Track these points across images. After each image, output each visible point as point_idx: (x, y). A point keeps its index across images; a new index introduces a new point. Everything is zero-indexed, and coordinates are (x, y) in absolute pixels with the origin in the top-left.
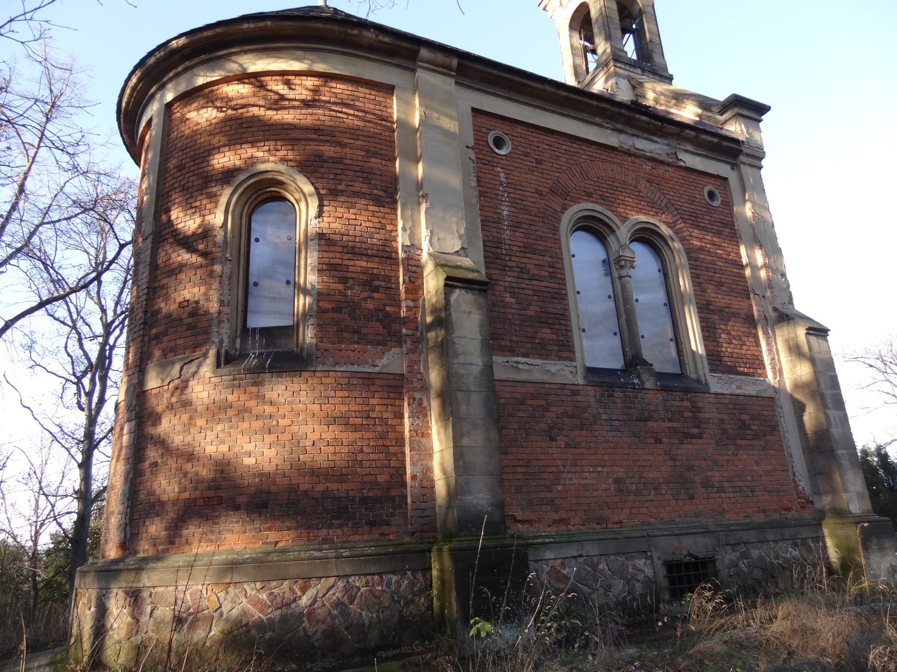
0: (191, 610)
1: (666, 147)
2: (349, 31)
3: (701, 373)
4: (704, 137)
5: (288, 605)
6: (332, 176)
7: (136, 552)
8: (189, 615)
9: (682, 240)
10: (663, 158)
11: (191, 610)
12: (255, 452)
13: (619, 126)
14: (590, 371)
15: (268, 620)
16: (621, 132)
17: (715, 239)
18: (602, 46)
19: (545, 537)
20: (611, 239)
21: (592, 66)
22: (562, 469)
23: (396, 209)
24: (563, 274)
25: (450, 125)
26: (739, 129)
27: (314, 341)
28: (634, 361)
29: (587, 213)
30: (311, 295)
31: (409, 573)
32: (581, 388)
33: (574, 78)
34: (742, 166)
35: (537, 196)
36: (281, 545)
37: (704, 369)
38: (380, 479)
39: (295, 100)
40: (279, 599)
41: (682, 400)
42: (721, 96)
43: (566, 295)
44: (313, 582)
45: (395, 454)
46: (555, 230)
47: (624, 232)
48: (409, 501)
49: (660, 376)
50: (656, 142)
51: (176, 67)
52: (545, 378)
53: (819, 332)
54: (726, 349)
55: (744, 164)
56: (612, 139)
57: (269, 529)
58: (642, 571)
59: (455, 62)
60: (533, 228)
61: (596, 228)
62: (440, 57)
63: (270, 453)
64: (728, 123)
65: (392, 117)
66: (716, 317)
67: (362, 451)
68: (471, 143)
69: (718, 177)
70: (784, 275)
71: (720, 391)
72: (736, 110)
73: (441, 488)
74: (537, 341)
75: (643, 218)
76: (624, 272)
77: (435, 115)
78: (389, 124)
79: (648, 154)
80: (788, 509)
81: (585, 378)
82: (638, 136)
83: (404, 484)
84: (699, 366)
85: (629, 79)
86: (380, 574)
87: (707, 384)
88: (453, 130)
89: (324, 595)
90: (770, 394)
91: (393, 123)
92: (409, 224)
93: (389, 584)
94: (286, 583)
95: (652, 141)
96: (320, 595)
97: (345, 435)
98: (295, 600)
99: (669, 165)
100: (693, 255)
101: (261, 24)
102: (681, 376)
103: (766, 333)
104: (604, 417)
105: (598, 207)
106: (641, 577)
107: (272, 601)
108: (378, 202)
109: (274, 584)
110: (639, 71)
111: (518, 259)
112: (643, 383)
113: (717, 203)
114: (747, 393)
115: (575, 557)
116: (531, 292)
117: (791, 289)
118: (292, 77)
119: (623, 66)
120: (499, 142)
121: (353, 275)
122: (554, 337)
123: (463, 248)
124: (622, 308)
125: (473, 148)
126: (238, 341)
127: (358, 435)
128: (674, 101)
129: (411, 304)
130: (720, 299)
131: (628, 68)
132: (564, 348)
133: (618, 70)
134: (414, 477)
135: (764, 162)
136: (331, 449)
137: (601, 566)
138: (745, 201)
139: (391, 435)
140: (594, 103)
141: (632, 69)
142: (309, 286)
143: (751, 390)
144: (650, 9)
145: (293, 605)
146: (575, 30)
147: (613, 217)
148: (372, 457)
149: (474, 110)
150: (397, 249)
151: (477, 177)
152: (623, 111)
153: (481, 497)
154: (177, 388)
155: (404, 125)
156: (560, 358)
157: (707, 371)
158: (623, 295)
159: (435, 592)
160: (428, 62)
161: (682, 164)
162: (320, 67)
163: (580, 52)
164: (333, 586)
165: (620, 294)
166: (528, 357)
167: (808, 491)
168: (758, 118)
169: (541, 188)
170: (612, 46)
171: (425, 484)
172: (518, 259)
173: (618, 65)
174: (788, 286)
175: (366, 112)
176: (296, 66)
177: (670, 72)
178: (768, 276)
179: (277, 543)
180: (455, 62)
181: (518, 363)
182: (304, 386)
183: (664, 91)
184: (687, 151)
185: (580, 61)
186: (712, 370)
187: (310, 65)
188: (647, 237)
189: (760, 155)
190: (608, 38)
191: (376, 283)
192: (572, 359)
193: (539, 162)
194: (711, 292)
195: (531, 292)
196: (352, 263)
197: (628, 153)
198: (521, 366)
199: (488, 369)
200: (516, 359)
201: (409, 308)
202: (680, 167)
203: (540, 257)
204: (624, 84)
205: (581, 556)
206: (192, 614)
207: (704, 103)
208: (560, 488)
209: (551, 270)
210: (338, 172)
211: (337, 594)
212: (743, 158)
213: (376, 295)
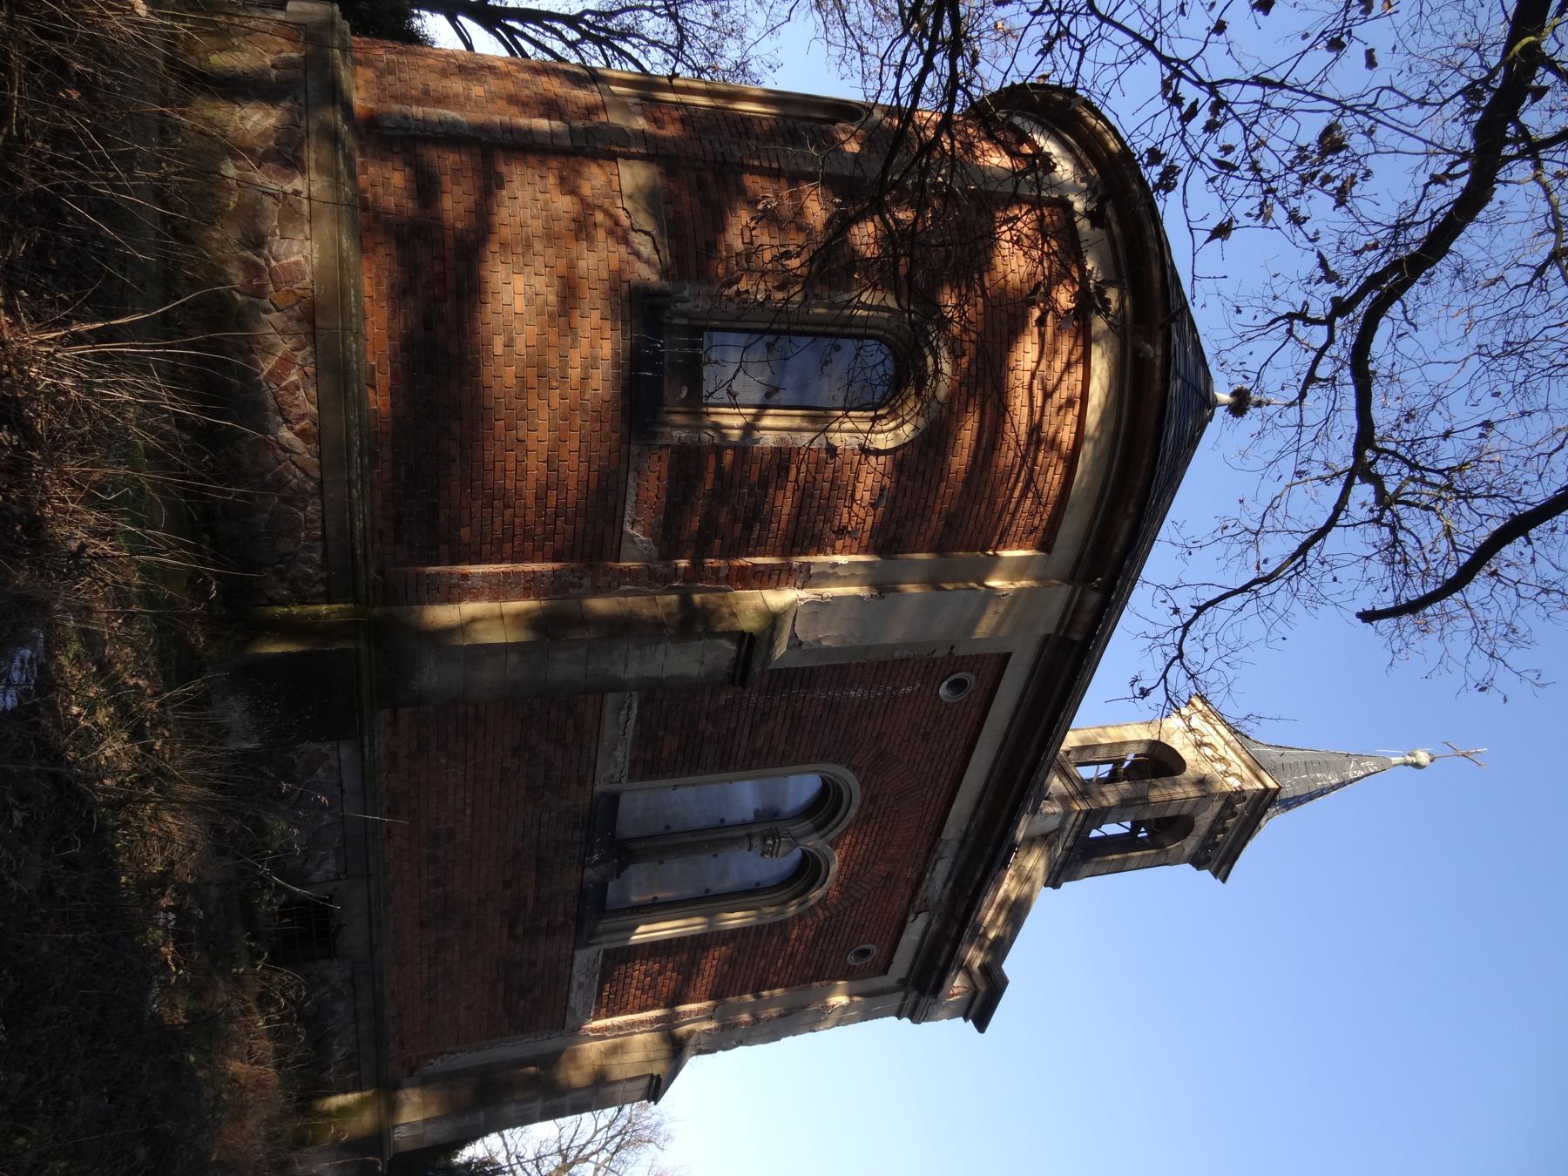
0: (273, 263)
1: (936, 898)
2: (1133, 501)
3: (604, 938)
4: (947, 948)
5: (280, 411)
6: (921, 467)
7: (353, 33)
8: (267, 260)
9: (800, 917)
10: (921, 894)
11: (273, 263)
12: (514, 293)
13: (970, 840)
14: (614, 799)
15: (259, 382)
16: (963, 842)
17: (799, 958)
18: (1111, 796)
19: (372, 745)
20: (807, 825)
22: (471, 763)
23: (865, 553)
24: (757, 767)
25: (984, 628)
27: (675, 441)
28: (624, 853)
29: (846, 797)
30: (743, 437)
31: (324, 575)
32: (589, 787)
33: (1077, 744)
34: (902, 994)
35: (875, 734)
36: (371, 393)
37: (610, 942)
38: (465, 532)
39: (1042, 414)
40: (289, 399)
41: (565, 915)
43: (727, 770)
44: (313, 446)
45: (500, 550)
46: (824, 757)
47: (813, 843)
48: (432, 569)
49: (603, 887)
50: (945, 886)
51: (1119, 224)
52: (606, 742)
53: (654, 1089)
54: (638, 971)
55: (905, 998)
56: (952, 830)
57: (394, 376)
58: (318, 867)
60: (828, 729)
61: (824, 807)
62: (1085, 618)
63: (509, 375)
65: (1004, 548)
66: (685, 957)
67: (506, 507)
68: (958, 652)
69: (890, 962)
70: (741, 1043)
71: (576, 962)
72: (982, 988)
73: (444, 614)
74: (661, 733)
75: (834, 868)
76: (757, 842)
77: (1001, 609)
78: (994, 544)
80: (402, 1044)
81: (603, 793)
82: (954, 863)
83: (456, 561)
84: (615, 936)
85: (1058, 831)
86: (323, 537)
87: (587, 945)
89: (294, 463)
90: (570, 1023)
91: (996, 549)
92: (841, 572)
93: (310, 549)
94: (314, 409)
95: (948, 880)
96: (295, 458)
97: (532, 484)
98: (287, 421)
99: (911, 901)
100: (778, 930)
101: (1157, 375)
102: (602, 910)
103: (658, 1019)
104: (545, 817)
105: (853, 811)
106: (309, 866)
107: (286, 388)
108: (876, 531)
109: (313, 392)
111: (782, 709)
112: (593, 866)
113: (851, 959)
114: (572, 995)
115: (341, 784)
116: (733, 725)
117: (720, 1053)
118: (1077, 411)
120: (958, 686)
121: (770, 496)
122: (665, 754)
123: (801, 643)
124: (705, 837)
125: (950, 654)
126: (684, 322)
127: (530, 502)
129: (722, 574)
130: (710, 965)
132: (647, 765)
133: (1074, 817)
134: (465, 576)
135: (906, 1021)
136: (511, 466)
137: (326, 817)
138: (850, 995)
139: (528, 545)
140: (1005, 812)
142: (757, 435)
143: (576, 1000)
145: (279, 419)
147: (845, 824)
148: (498, 520)
149: (1007, 656)
150: (807, 554)
151: (908, 659)
152: (990, 849)
153: (432, 676)
154: (617, 223)
155: (992, 564)
156: (633, 763)
157: (607, 946)
158: (723, 839)
159: (296, 610)
160: (1081, 601)
162: (1087, 448)
163: (1115, 755)
164: (307, 475)
165: (726, 835)
166: (637, 721)
167: (429, 1069)
168: (973, 1010)
169: (886, 739)
171: (455, 592)
172: (782, 709)
174: (724, 1049)
175: (1014, 514)
176: (1092, 419)
178: (740, 1024)
179: (374, 387)
180: (1077, 637)
181: (630, 708)
182: (607, 427)
184: (929, 924)
185: (1102, 754)
186: (607, 953)
187: (1092, 438)
188: (807, 871)
189: (917, 1014)
191: (757, 527)
192: (632, 777)
193: (926, 737)
194: (718, 952)
195: (733, 725)
196: (789, 494)
197: (931, 850)
198: (624, 712)
199: (618, 686)
200: (635, 706)
201: (716, 570)
202: (906, 916)
203: (784, 736)
205: (343, 792)
206: (268, 265)
207: (1000, 948)
208: (443, 761)
209: (765, 750)
210: (928, 476)
211: (295, 478)
213: (739, 526)
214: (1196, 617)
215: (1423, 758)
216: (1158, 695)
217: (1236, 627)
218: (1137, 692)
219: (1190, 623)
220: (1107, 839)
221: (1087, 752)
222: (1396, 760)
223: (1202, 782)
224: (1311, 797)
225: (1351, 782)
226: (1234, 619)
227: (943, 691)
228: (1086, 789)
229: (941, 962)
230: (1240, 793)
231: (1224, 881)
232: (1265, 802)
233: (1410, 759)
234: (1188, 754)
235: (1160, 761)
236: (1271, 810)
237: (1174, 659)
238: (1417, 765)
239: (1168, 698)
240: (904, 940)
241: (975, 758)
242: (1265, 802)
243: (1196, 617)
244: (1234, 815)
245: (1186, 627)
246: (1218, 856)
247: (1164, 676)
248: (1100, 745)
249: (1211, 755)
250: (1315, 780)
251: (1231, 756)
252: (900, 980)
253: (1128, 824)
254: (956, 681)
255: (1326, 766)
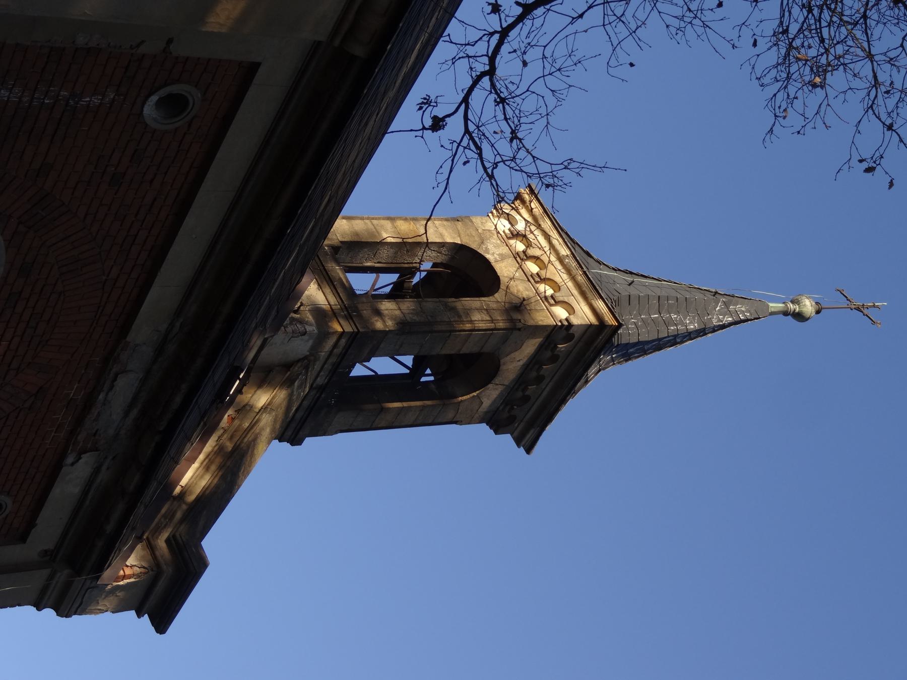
21: (361, 283)
25: (222, 18)
26: (128, 571)
34: (45, 572)
42: (211, 544)
50: (126, 414)
55: (51, 577)
56: (145, 331)
59: (359, 51)
64: (147, 553)
69: (31, 524)
72: (168, 570)
79: (101, 397)
85: (306, 361)
88: (212, 19)
110: (320, 381)
119: (337, 351)
120: (174, 105)
128: (229, 446)
131: (333, 360)
135: (49, 613)
141: (328, 367)
144: (450, 415)
146: (452, 258)
149: (254, 67)
161: (70, 459)
163: (407, 260)
168: (153, 600)
170: (385, 333)
173: (343, 341)
177: (308, 441)
180: (359, 51)
183: (257, 429)
184: (97, 471)
190: (404, 327)
204: (301, 347)
212: (63, 575)
214: (520, 19)
215: (808, 306)
216: (454, 128)
217: (571, 38)
218: (428, 122)
219: (512, 26)
220: (376, 379)
221: (357, 250)
222: (775, 306)
223: (519, 307)
224: (659, 345)
225: (714, 330)
226: (571, 29)
227: (149, 110)
228: (352, 306)
229: (109, 528)
230: (566, 329)
231: (528, 450)
232: (594, 346)
233: (791, 306)
234: (505, 269)
235: (467, 272)
236: (605, 358)
237: (483, 74)
238: (799, 317)
239: (467, 131)
240: (57, 492)
241: (190, 221)
242: (594, 346)
243: (520, 19)
244: (554, 359)
245: (504, 33)
246: (524, 417)
247: (466, 100)
248: (382, 243)
249: (534, 266)
250: (667, 324)
251: (561, 277)
252: (45, 552)
253: (408, 360)
254: (170, 96)
255: (685, 305)
